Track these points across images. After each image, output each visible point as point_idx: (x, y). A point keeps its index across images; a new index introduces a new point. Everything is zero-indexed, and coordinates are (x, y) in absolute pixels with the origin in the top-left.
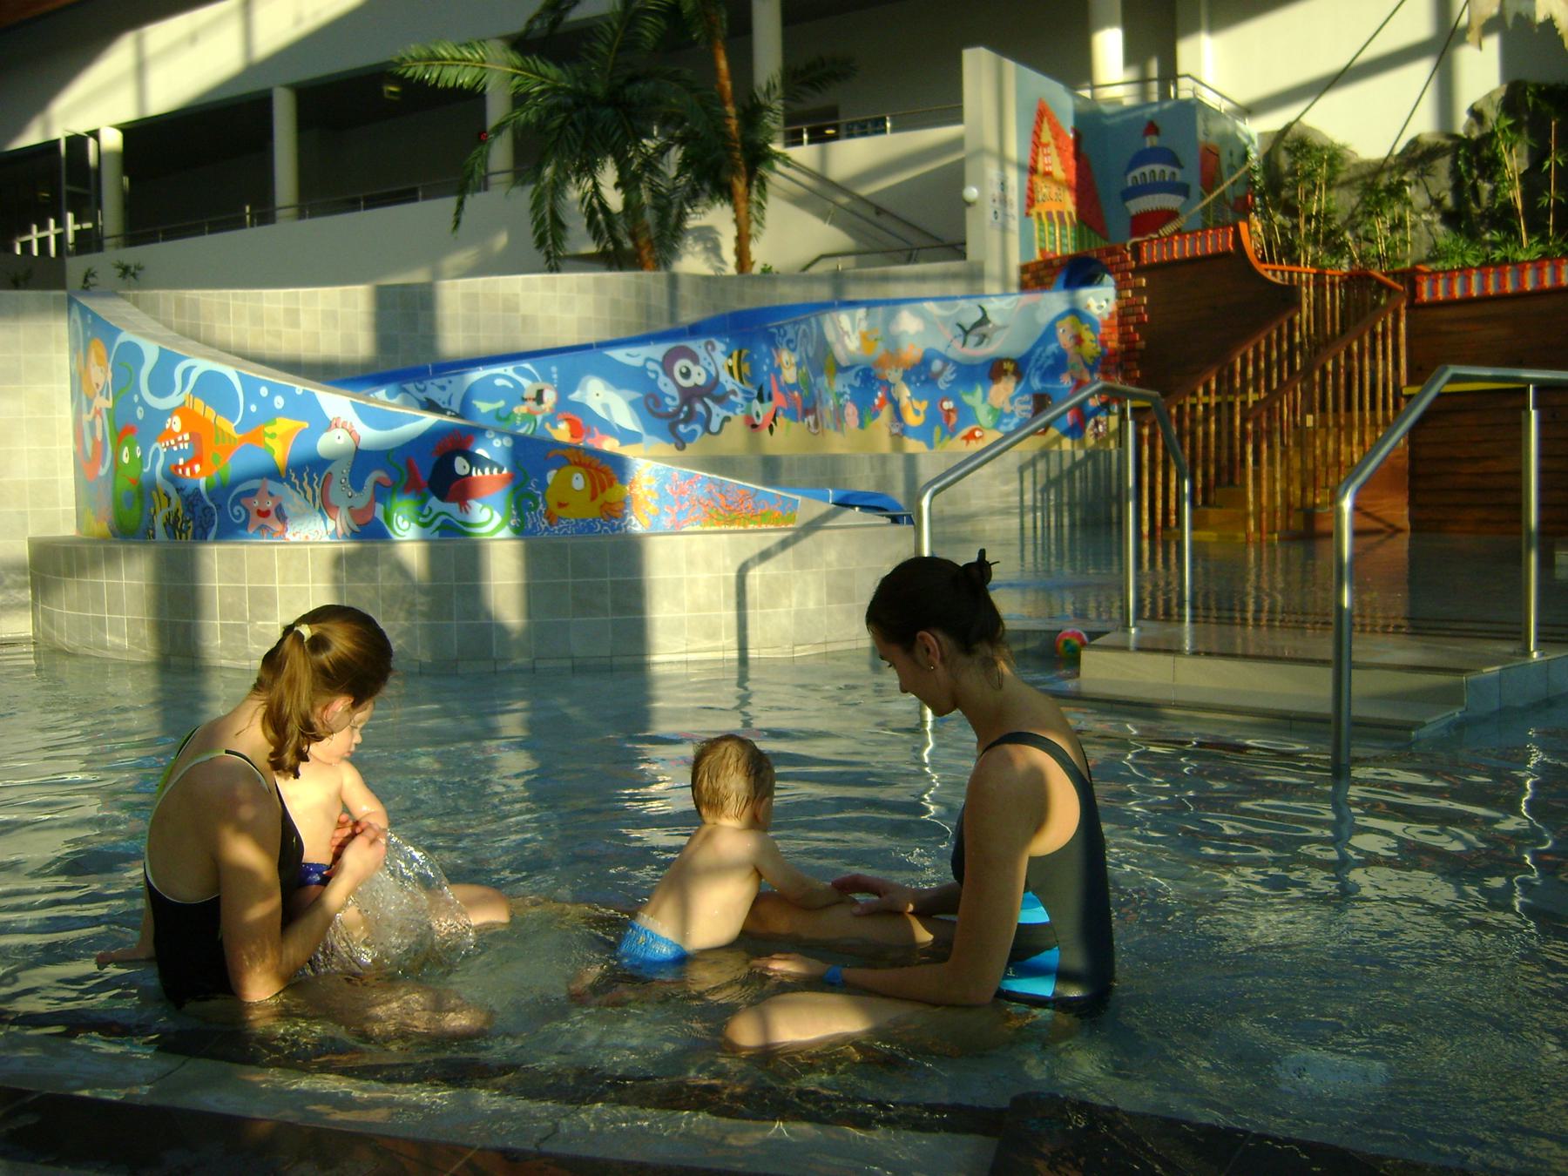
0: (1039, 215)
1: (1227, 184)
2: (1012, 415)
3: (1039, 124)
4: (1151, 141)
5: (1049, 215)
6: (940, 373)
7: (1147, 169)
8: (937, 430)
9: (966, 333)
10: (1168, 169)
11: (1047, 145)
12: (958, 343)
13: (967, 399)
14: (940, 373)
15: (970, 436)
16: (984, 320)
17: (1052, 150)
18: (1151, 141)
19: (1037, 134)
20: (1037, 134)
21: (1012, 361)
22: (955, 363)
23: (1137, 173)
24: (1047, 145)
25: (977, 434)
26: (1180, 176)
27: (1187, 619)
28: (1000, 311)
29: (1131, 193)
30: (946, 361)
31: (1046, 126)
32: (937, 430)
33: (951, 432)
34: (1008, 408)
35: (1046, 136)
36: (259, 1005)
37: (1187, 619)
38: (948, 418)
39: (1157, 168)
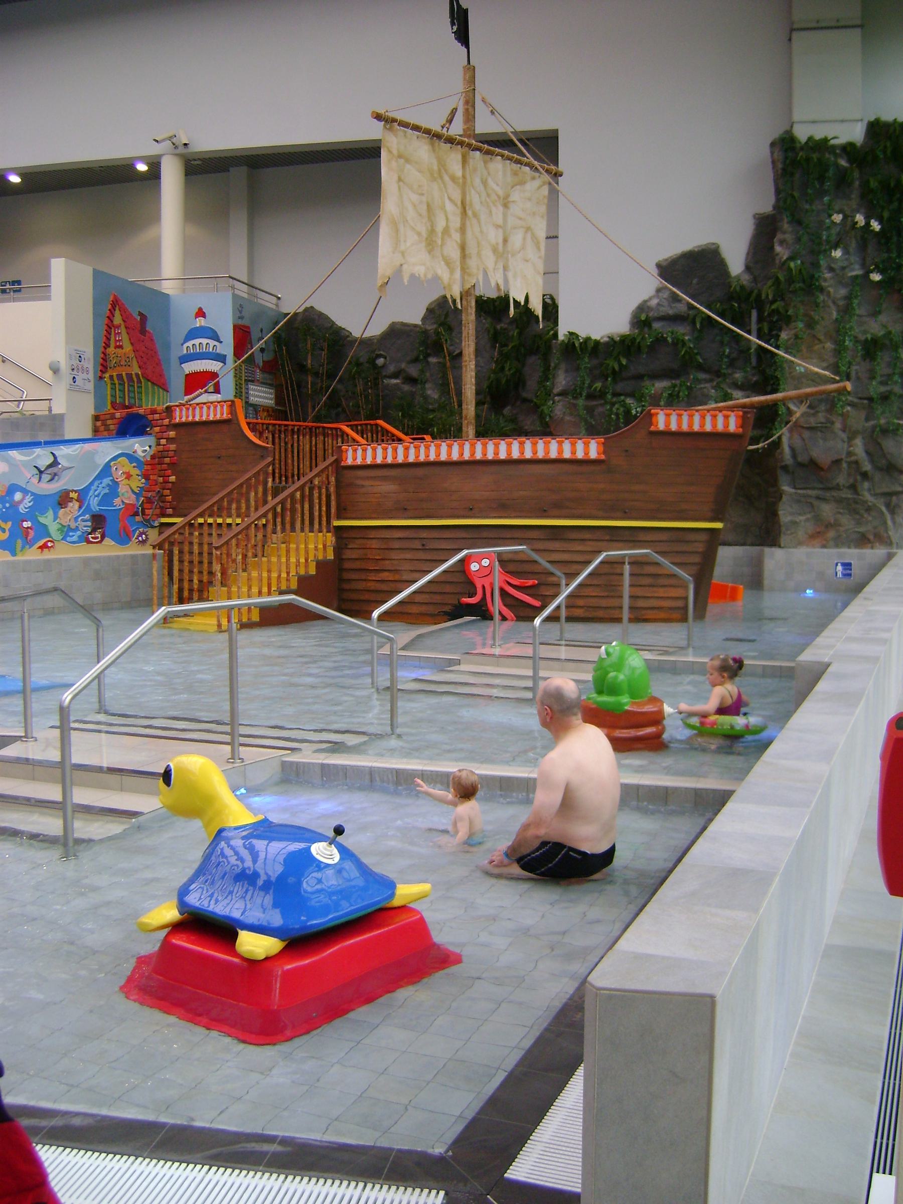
0: (111, 377)
1: (256, 347)
2: (77, 528)
3: (112, 311)
4: (200, 322)
5: (120, 377)
6: (21, 502)
7: (197, 342)
8: (19, 543)
9: (41, 472)
10: (212, 343)
11: (118, 327)
12: (35, 480)
13: (42, 520)
14: (21, 502)
15: (44, 547)
16: (55, 463)
17: (123, 330)
18: (200, 322)
19: (110, 318)
20: (110, 318)
21: (76, 491)
22: (33, 494)
23: (190, 344)
24: (118, 327)
25: (50, 544)
26: (220, 349)
27: (793, 359)
28: (67, 457)
29: (185, 359)
30: (25, 492)
31: (117, 313)
32: (19, 543)
33: (29, 543)
34: (73, 525)
35: (118, 319)
36: (631, 655)
37: (793, 359)
38: (27, 534)
39: (205, 341)
